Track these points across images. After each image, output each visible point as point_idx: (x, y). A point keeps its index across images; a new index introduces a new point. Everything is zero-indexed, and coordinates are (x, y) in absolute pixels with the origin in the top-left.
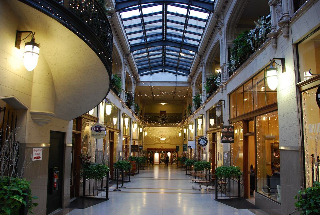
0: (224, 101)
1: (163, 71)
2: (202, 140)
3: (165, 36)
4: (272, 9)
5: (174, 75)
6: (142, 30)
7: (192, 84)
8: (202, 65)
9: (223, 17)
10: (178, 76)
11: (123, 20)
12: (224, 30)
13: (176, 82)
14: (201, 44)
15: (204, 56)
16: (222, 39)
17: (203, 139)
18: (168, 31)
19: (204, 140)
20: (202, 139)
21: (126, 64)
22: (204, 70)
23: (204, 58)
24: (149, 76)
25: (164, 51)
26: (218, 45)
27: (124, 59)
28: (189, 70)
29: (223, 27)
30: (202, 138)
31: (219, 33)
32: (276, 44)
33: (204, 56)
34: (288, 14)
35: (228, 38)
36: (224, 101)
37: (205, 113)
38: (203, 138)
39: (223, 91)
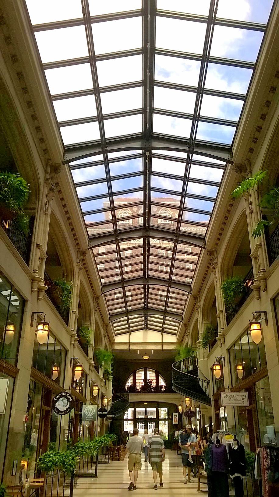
0: (224, 357)
1: (144, 328)
2: (61, 399)
3: (147, 304)
4: (254, 261)
5: (159, 334)
6: (113, 230)
7: (187, 335)
8: (197, 310)
9: (200, 299)
10: (165, 335)
11: (87, 226)
12: (218, 270)
13: (162, 343)
14: (187, 304)
15: (217, 253)
16: (250, 206)
17: (66, 397)
18: (151, 273)
19: (65, 401)
20: (62, 396)
21: (105, 336)
22: (217, 276)
23: (200, 301)
24: (127, 335)
25: (146, 291)
26: (212, 289)
27: (104, 331)
28: (181, 315)
29: (189, 335)
30: (63, 396)
31: (244, 198)
32: (225, 342)
33: (217, 253)
34: (265, 269)
35: (204, 319)
36: (224, 357)
37: (225, 354)
38: (64, 394)
39: (222, 345)
